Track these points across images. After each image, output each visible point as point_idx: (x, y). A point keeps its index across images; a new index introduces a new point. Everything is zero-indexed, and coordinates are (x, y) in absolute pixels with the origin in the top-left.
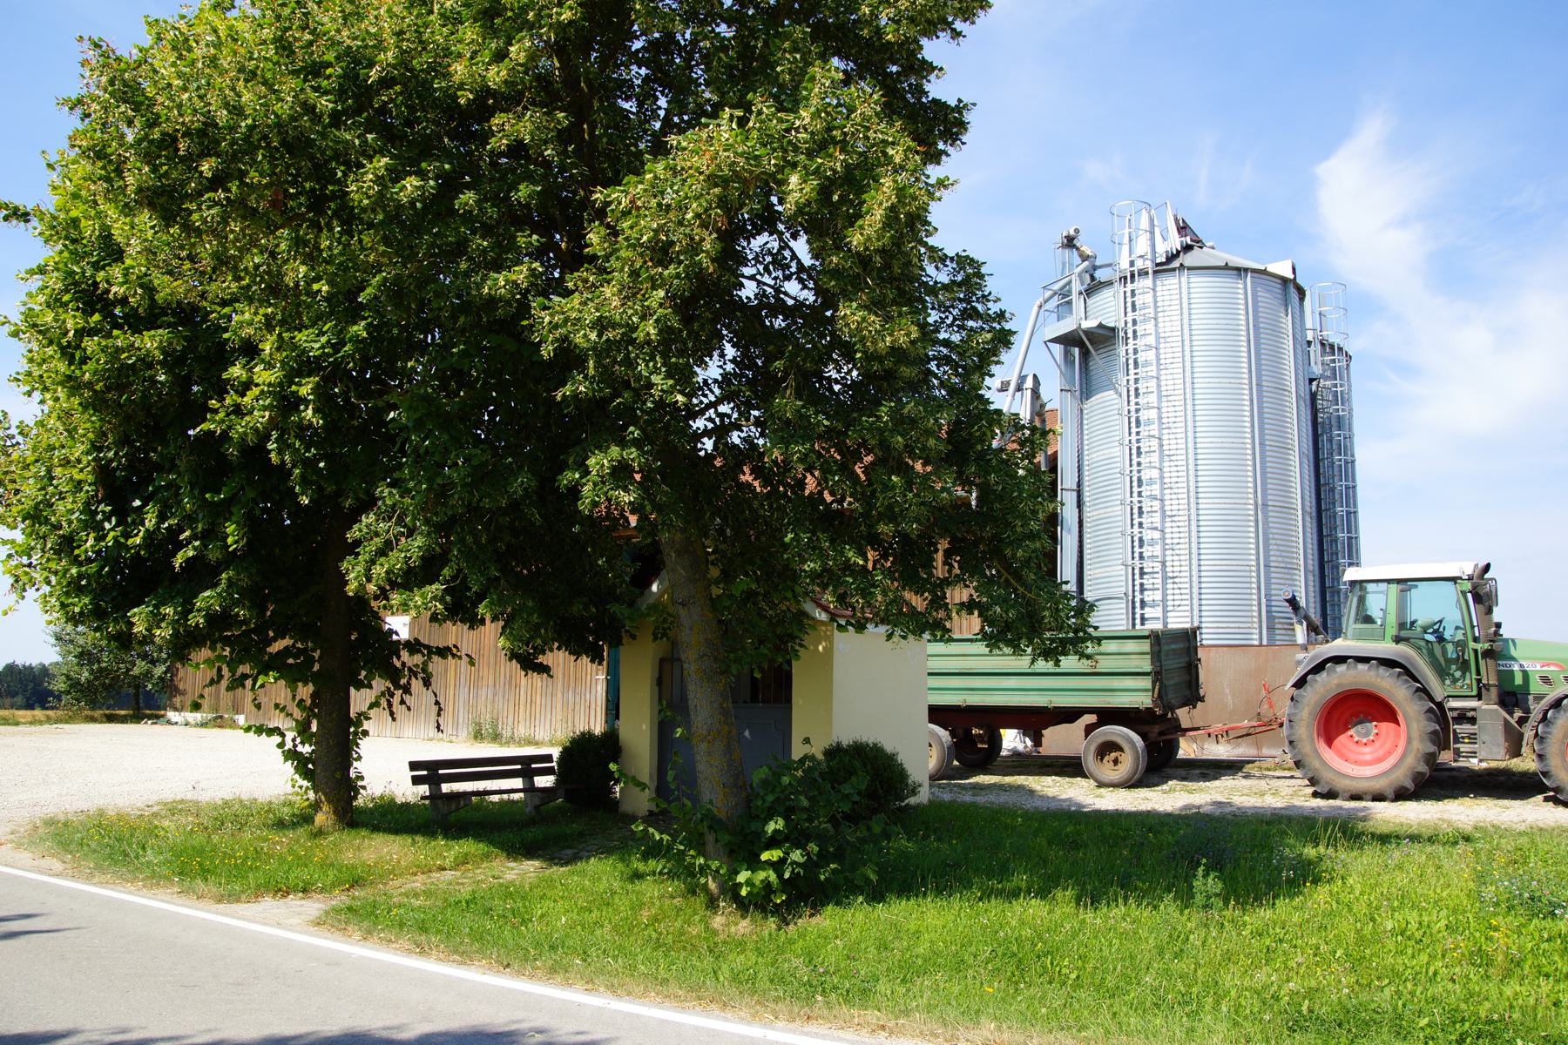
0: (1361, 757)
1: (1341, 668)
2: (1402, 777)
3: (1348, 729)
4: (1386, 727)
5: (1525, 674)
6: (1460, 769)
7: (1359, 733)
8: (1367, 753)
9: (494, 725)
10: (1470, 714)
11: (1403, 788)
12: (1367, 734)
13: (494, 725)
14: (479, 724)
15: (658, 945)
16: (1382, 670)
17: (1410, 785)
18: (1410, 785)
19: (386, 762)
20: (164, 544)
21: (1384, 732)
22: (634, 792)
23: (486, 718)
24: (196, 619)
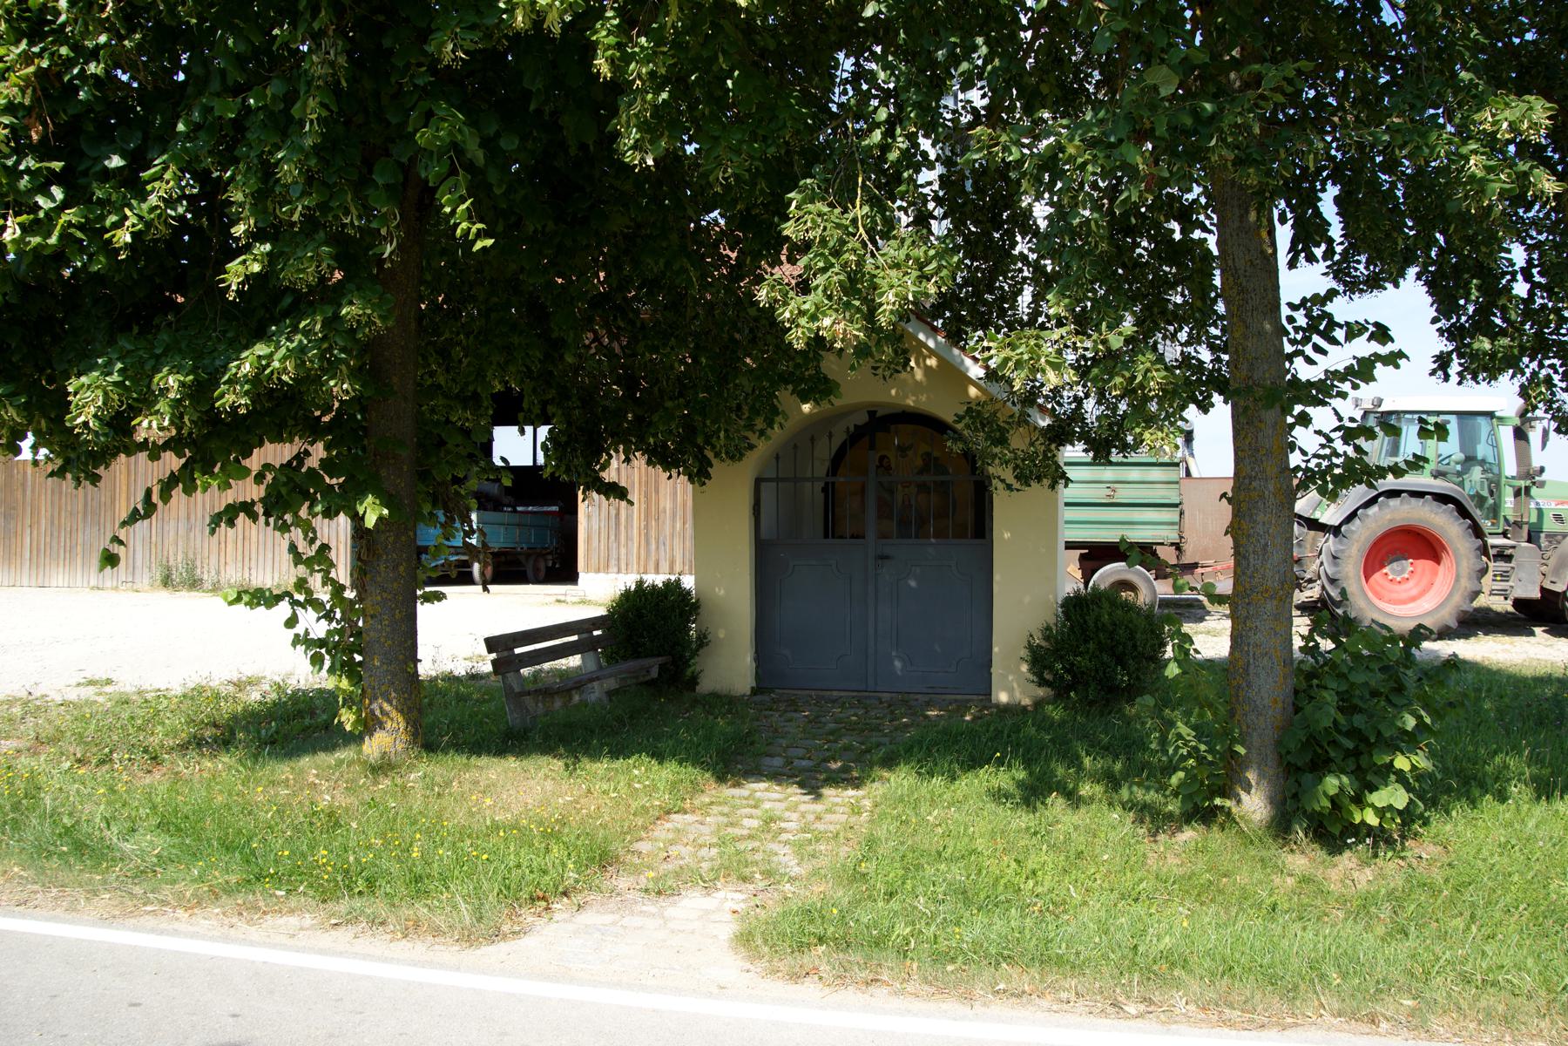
0: (1395, 596)
1: (1394, 502)
2: (1448, 617)
3: (1383, 566)
4: (1424, 565)
5: (1540, 512)
6: (1476, 610)
7: (1393, 570)
8: (1411, 588)
9: (191, 569)
10: (1508, 552)
11: (1448, 627)
12: (1403, 571)
13: (191, 569)
14: (169, 568)
15: (1467, 980)
16: (1413, 500)
17: (1453, 624)
18: (1453, 624)
19: (458, 629)
20: (198, 242)
21: (1419, 570)
22: (731, 664)
23: (177, 561)
24: (231, 398)
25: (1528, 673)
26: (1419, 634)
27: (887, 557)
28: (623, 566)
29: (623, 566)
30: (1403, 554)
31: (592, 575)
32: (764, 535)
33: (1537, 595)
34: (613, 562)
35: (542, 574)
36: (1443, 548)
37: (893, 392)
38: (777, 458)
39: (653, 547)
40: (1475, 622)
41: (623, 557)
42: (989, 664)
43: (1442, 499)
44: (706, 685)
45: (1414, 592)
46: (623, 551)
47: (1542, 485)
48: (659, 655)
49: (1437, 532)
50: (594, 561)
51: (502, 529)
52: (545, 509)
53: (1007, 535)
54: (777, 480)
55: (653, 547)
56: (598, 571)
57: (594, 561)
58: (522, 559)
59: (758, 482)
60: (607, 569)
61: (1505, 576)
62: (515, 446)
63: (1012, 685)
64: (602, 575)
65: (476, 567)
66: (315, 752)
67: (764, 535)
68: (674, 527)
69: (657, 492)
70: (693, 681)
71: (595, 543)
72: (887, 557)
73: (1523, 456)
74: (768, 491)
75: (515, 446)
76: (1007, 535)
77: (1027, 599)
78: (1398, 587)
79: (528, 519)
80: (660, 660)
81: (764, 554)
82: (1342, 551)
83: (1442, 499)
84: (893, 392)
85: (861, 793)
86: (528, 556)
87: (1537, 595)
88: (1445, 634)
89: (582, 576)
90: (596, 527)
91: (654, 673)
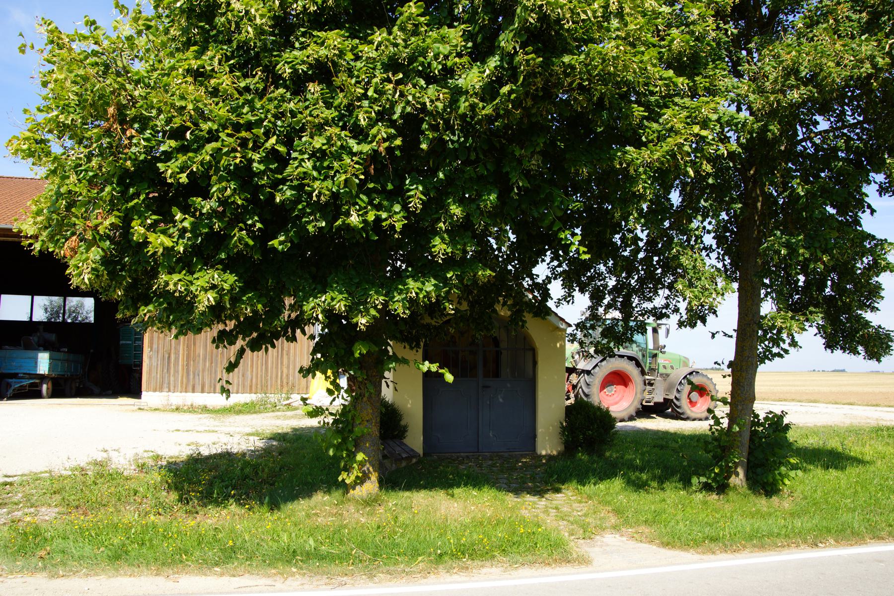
4: (621, 388)
25: (686, 433)
28: (172, 388)
29: (190, 388)
31: (151, 393)
33: (662, 400)
34: (165, 385)
36: (630, 380)
39: (191, 377)
40: (645, 411)
41: (172, 382)
42: (534, 436)
43: (631, 358)
45: (618, 399)
46: (172, 379)
47: (664, 353)
49: (628, 373)
50: (153, 385)
55: (191, 377)
56: (155, 391)
57: (153, 385)
60: (161, 390)
61: (650, 392)
62: (344, 322)
63: (548, 444)
64: (157, 393)
65: (45, 387)
66: (310, 496)
68: (205, 365)
69: (195, 344)
71: (154, 374)
73: (656, 340)
75: (344, 322)
77: (553, 406)
78: (609, 398)
83: (631, 358)
85: (519, 500)
87: (662, 400)
88: (631, 418)
89: (144, 394)
90: (154, 364)
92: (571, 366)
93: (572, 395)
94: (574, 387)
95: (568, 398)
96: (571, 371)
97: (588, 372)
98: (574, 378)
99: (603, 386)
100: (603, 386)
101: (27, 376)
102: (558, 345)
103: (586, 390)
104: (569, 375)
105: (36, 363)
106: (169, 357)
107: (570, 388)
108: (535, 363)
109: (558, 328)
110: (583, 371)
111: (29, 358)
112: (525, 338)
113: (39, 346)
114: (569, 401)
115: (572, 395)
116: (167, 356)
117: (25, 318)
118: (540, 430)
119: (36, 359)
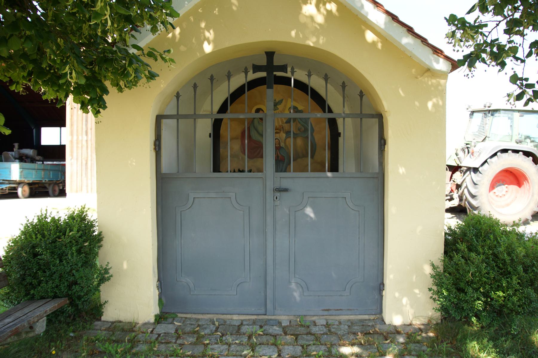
16: (514, 154)
18: (530, 218)
26: (515, 224)
27: (286, 190)
30: (504, 182)
32: (164, 169)
35: (57, 193)
36: (526, 179)
37: (293, 33)
38: (178, 96)
42: (381, 287)
43: (527, 154)
44: (110, 314)
48: (55, 297)
51: (34, 172)
52: (55, 163)
53: (402, 170)
54: (177, 117)
58: (47, 185)
59: (159, 119)
67: (164, 169)
70: (96, 311)
72: (286, 190)
74: (168, 125)
76: (402, 170)
79: (49, 167)
80: (50, 307)
81: (163, 182)
82: (480, 181)
83: (527, 154)
84: (293, 33)
86: (50, 184)
91: (41, 327)
92: (455, 164)
93: (456, 196)
94: (458, 187)
95: (451, 199)
96: (454, 169)
97: (476, 170)
98: (458, 177)
99: (493, 186)
100: (493, 186)
101: (7, 182)
102: (430, 104)
103: (473, 191)
104: (453, 173)
105: (10, 172)
106: (87, 163)
107: (454, 188)
108: (382, 142)
109: (429, 71)
110: (469, 169)
111: (5, 168)
112: (361, 95)
113: (16, 159)
114: (452, 202)
115: (456, 196)
116: (84, 162)
117: (59, 144)
118: (390, 277)
119: (10, 169)
